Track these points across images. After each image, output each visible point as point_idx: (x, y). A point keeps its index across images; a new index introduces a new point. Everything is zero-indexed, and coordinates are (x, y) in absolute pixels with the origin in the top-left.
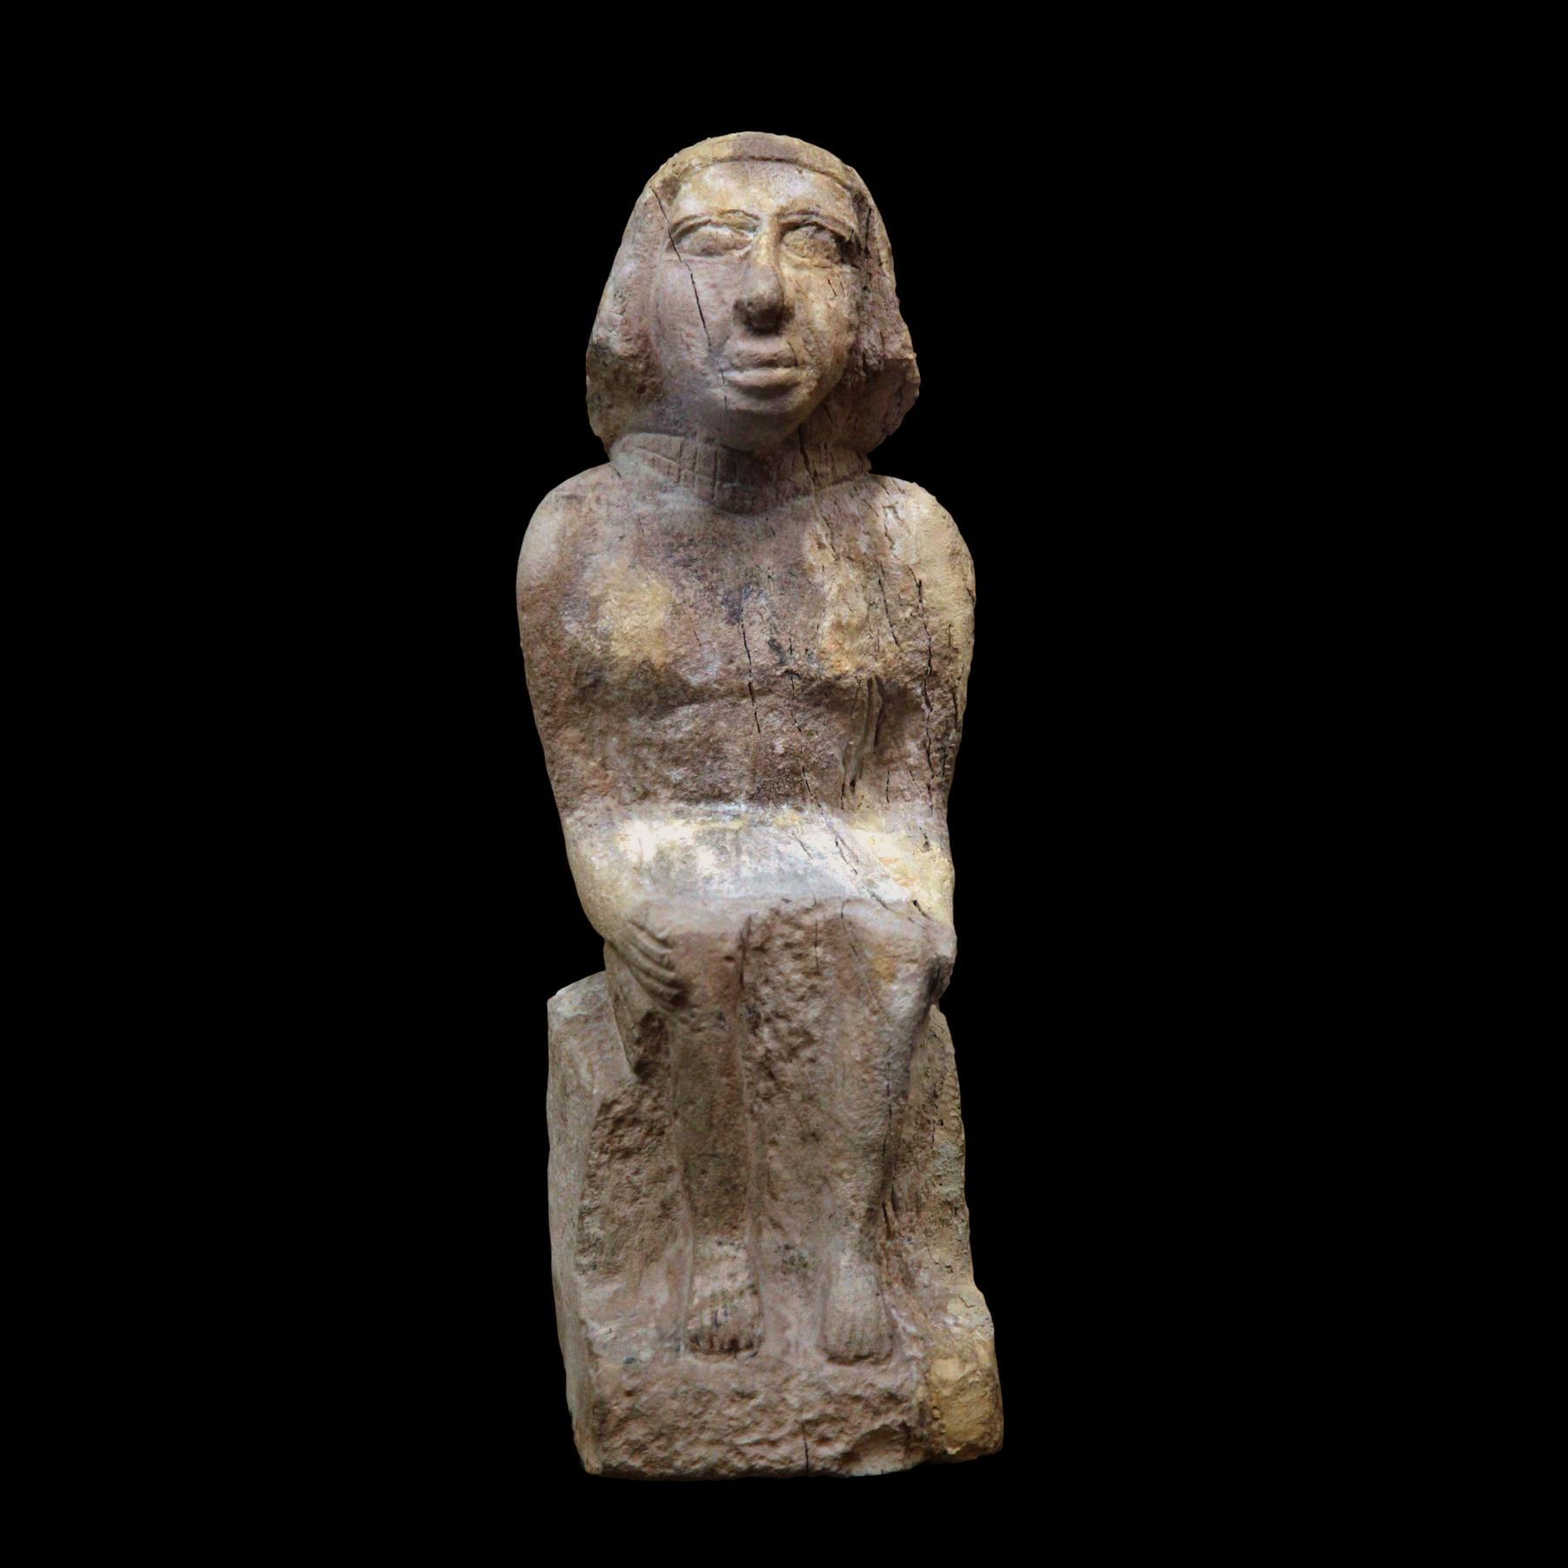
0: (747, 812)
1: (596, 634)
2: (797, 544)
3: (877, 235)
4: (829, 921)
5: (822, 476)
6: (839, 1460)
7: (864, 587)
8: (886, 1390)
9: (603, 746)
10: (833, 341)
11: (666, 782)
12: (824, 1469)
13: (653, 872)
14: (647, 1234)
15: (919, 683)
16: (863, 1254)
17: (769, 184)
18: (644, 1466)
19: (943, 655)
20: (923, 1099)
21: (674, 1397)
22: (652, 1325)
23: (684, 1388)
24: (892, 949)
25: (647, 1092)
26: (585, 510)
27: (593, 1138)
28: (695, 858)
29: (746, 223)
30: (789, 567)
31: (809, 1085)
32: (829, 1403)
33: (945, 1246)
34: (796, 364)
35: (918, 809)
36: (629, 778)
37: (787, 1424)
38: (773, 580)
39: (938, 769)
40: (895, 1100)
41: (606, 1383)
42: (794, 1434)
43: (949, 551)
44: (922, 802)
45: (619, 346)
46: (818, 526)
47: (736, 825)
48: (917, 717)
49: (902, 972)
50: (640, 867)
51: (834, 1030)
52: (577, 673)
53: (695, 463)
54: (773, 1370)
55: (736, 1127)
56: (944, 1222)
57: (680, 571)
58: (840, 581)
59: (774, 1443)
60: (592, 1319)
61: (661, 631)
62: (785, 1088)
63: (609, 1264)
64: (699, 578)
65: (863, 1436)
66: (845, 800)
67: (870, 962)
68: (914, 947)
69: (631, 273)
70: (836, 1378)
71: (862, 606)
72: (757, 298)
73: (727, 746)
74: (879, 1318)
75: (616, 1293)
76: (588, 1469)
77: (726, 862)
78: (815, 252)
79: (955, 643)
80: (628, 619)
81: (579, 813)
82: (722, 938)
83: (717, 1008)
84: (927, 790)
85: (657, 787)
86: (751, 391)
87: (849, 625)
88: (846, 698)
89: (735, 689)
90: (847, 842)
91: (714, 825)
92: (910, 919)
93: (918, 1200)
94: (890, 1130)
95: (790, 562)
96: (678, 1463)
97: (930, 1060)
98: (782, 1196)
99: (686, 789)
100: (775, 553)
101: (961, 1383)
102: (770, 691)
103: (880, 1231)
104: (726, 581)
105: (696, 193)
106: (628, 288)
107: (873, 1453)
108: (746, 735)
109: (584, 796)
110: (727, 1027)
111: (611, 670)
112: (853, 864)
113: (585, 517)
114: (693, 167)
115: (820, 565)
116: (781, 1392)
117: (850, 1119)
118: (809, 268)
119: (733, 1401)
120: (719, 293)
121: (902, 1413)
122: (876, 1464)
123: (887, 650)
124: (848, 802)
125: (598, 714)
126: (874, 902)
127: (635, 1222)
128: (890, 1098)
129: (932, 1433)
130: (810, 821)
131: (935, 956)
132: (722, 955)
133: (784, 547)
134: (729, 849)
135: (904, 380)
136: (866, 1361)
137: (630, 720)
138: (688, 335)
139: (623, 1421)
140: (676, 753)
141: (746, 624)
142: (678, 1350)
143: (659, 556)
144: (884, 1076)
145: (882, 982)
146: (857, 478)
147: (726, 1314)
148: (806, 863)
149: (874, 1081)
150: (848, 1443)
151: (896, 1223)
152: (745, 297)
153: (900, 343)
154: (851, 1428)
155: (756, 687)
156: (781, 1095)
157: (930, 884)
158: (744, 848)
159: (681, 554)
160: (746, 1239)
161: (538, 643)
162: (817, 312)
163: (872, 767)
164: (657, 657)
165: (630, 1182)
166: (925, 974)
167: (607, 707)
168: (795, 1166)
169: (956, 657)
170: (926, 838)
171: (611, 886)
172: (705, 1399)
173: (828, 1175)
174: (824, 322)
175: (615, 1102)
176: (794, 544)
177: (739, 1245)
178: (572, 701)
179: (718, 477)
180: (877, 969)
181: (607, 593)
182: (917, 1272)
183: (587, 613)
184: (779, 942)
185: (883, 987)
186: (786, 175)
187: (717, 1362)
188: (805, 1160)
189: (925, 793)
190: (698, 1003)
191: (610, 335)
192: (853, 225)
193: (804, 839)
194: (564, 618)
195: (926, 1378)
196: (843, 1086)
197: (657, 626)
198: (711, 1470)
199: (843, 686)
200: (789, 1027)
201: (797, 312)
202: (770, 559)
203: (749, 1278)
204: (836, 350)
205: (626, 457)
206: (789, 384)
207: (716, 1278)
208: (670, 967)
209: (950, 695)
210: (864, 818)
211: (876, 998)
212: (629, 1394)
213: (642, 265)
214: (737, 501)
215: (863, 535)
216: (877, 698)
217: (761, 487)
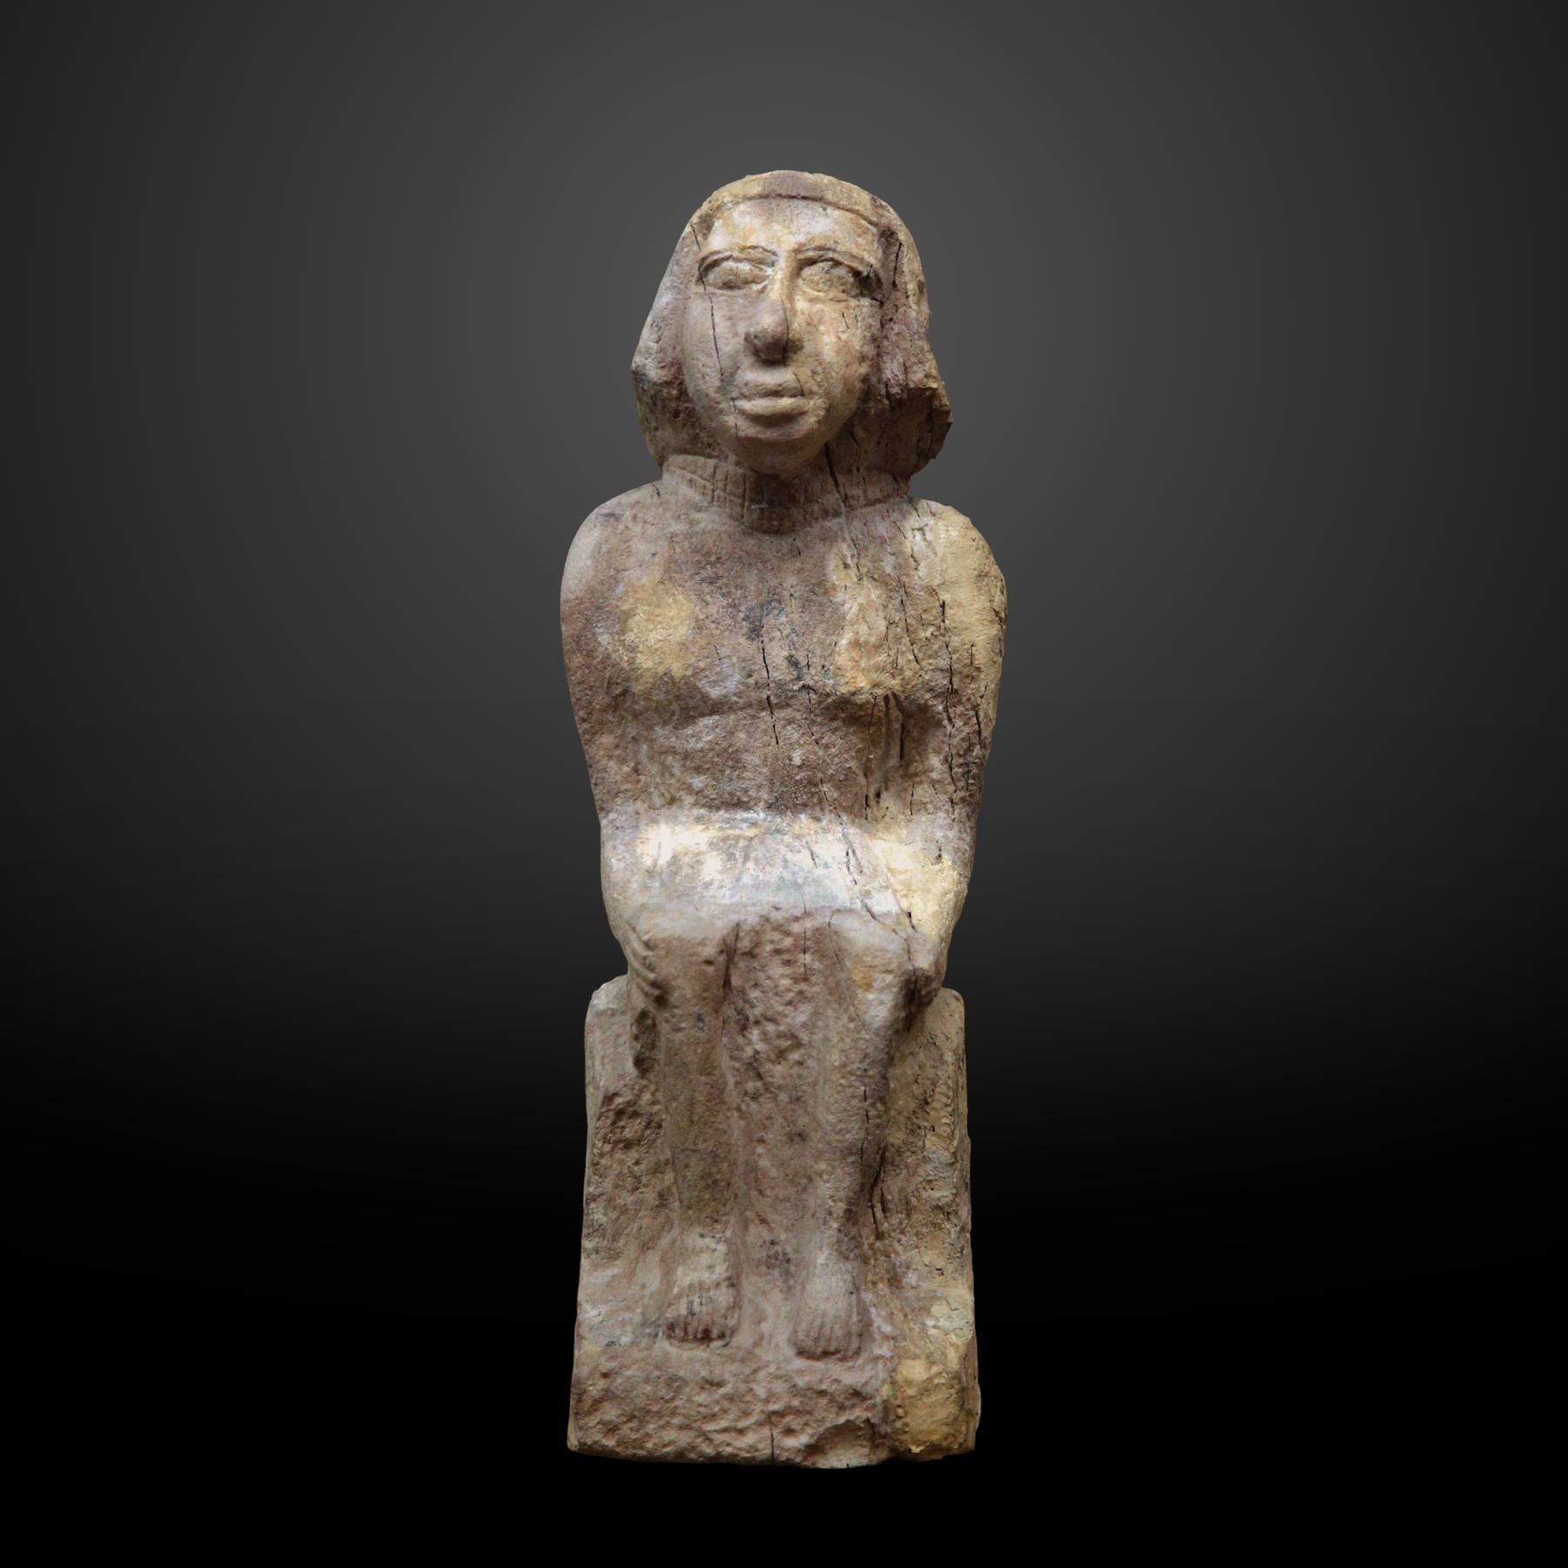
0: (765, 820)
2: (821, 564)
3: (906, 269)
4: (817, 930)
5: (853, 498)
6: (803, 1451)
7: (885, 607)
8: (851, 1386)
9: (636, 753)
10: (842, 372)
11: (689, 789)
12: (788, 1459)
13: (663, 875)
14: (645, 1222)
15: (940, 700)
16: (841, 1253)
17: (792, 221)
18: (618, 1445)
19: (964, 674)
20: (912, 1105)
21: (647, 1381)
22: (639, 1310)
23: (657, 1373)
24: (868, 959)
25: (646, 1086)
26: (621, 527)
27: (597, 1128)
29: (763, 259)
30: (811, 586)
31: (796, 1087)
32: (796, 1396)
33: (937, 1248)
34: (803, 394)
35: (940, 822)
36: (658, 784)
37: (754, 1414)
38: (795, 598)
39: (961, 784)
40: (873, 1105)
41: (584, 1364)
42: (761, 1424)
43: (976, 573)
44: (944, 815)
45: (654, 373)
46: (845, 546)
47: (751, 833)
48: (940, 733)
49: (878, 981)
50: (653, 871)
51: (820, 1035)
52: (609, 683)
53: (726, 485)
54: (743, 1360)
56: (936, 1226)
57: (706, 588)
58: (861, 600)
59: (741, 1432)
60: (587, 1302)
61: (683, 645)
62: (772, 1089)
63: (610, 1249)
64: (723, 595)
65: (827, 1430)
66: (869, 811)
67: (849, 970)
68: (890, 958)
69: (667, 304)
70: (803, 1372)
71: (882, 625)
72: (762, 332)
73: (746, 757)
74: (850, 1316)
75: (613, 1277)
76: (569, 1445)
77: (730, 869)
78: (831, 286)
79: (977, 662)
80: (654, 632)
81: (612, 816)
82: (703, 943)
83: (696, 1009)
84: (950, 803)
85: (681, 793)
86: (757, 419)
87: (867, 643)
88: (862, 713)
89: (754, 702)
90: (858, 853)
91: (730, 832)
92: (894, 931)
93: (908, 1203)
94: (868, 1134)
95: (813, 581)
96: (649, 1445)
97: (920, 1067)
98: (768, 1192)
100: (799, 572)
101: (926, 1384)
102: (788, 705)
103: (866, 1231)
104: (749, 598)
105: (724, 229)
106: (664, 318)
107: (839, 1446)
108: (764, 746)
109: (617, 799)
110: (705, 1028)
111: (637, 680)
112: (855, 875)
113: (621, 534)
114: (725, 204)
115: (843, 584)
116: (748, 1382)
117: (828, 1122)
118: (824, 302)
119: (703, 1388)
120: (734, 325)
121: (867, 1409)
122: (842, 1458)
123: (905, 667)
124: (872, 813)
125: (629, 722)
126: (864, 912)
127: (635, 1210)
128: (867, 1103)
129: (896, 1431)
130: (826, 831)
131: (911, 968)
132: (700, 959)
133: (808, 567)
134: (737, 856)
135: (931, 408)
136: (833, 1357)
137: (656, 728)
139: (597, 1403)
140: (697, 762)
141: (766, 639)
142: (656, 1335)
143: (687, 573)
144: (861, 1081)
145: (859, 992)
146: (892, 500)
148: (809, 872)
149: (851, 1086)
150: (812, 1436)
151: (886, 1225)
152: (752, 330)
154: (817, 1421)
155: (774, 700)
156: (769, 1095)
157: (931, 896)
158: (753, 855)
159: (709, 571)
160: (728, 1233)
161: (574, 653)
162: (827, 344)
163: (899, 780)
164: (677, 669)
165: (631, 1172)
166: (900, 985)
167: (636, 715)
168: (782, 1164)
169: (978, 676)
170: (940, 850)
171: (622, 888)
172: (676, 1384)
175: (616, 1094)
176: (819, 564)
177: (720, 1238)
178: (603, 710)
179: (747, 498)
180: (855, 978)
181: (636, 608)
182: (905, 1273)
183: (618, 626)
184: (769, 948)
185: (859, 996)
186: (810, 212)
187: (691, 1349)
188: (791, 1159)
189: (948, 806)
190: (677, 1004)
191: (647, 362)
192: (872, 260)
193: (816, 848)
195: (891, 1377)
197: (679, 640)
198: (681, 1454)
199: (859, 702)
200: (777, 1030)
201: (806, 344)
202: (794, 578)
203: (727, 1269)
204: (845, 380)
205: (669, 477)
206: (795, 412)
207: (695, 1270)
208: (651, 968)
209: (972, 713)
210: (887, 829)
211: (854, 1005)
212: (605, 1376)
213: (679, 296)
214: (765, 522)
215: (889, 556)
216: (895, 713)
217: (788, 509)
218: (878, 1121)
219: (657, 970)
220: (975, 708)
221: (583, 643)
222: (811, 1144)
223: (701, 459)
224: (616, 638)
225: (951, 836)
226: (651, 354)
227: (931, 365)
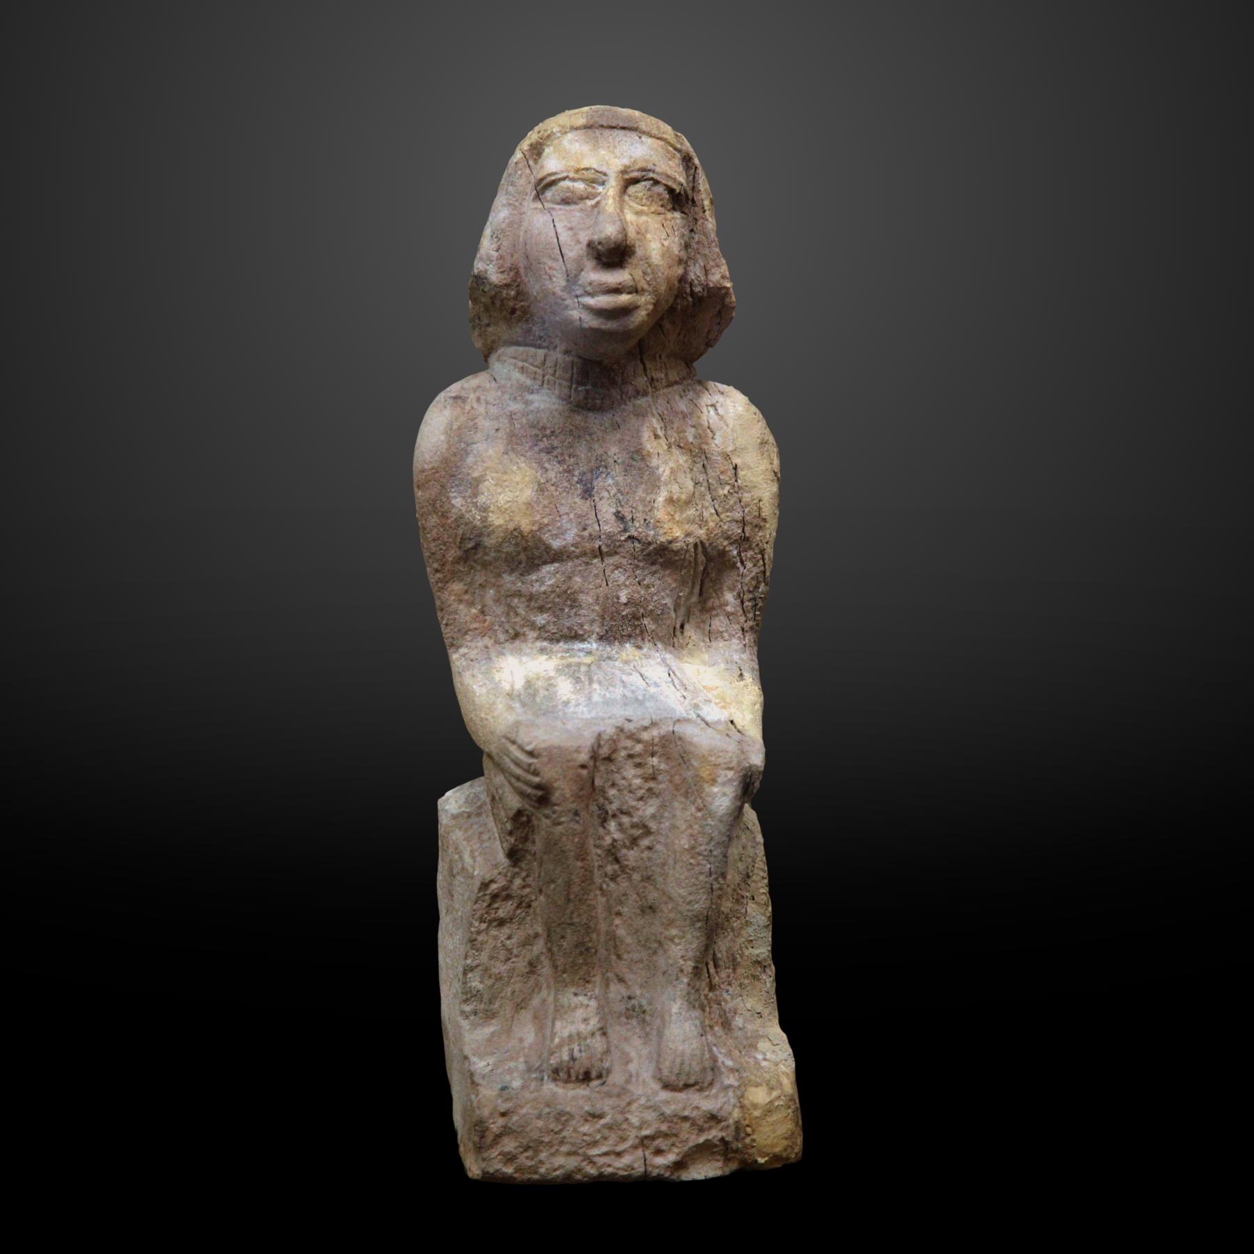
0: (597, 649)
1: (476, 507)
2: (637, 435)
3: (701, 188)
4: (663, 737)
5: (657, 381)
6: (671, 1168)
7: (691, 470)
8: (709, 1112)
9: (482, 597)
10: (666, 273)
11: (533, 626)
12: (659, 1175)
13: (522, 697)
14: (517, 987)
15: (735, 546)
16: (690, 1003)
17: (615, 147)
18: (515, 1172)
19: (754, 524)
20: (738, 879)
21: (539, 1117)
22: (522, 1060)
23: (547, 1110)
24: (713, 759)
25: (517, 873)
26: (468, 408)
27: (474, 910)
29: (597, 178)
30: (631, 454)
31: (647, 868)
32: (663, 1122)
33: (755, 996)
34: (636, 291)
35: (734, 647)
36: (503, 622)
37: (629, 1139)
38: (618, 464)
39: (751, 615)
40: (716, 879)
41: (485, 1106)
42: (635, 1147)
43: (759, 441)
44: (738, 642)
45: (495, 277)
46: (654, 421)
47: (588, 660)
48: (734, 574)
49: (722, 777)
50: (512, 694)
51: (667, 824)
52: (461, 539)
53: (555, 371)
54: (619, 1096)
56: (755, 977)
57: (544, 456)
58: (672, 464)
59: (619, 1154)
60: (474, 1055)
61: (529, 505)
62: (628, 870)
63: (487, 1011)
64: (559, 462)
65: (690, 1148)
66: (675, 640)
67: (696, 769)
68: (731, 758)
69: (504, 219)
70: (669, 1102)
71: (690, 485)
72: (606, 239)
73: (582, 597)
74: (703, 1054)
75: (493, 1034)
76: (470, 1175)
77: (580, 689)
78: (652, 201)
79: (764, 514)
80: (502, 495)
81: (463, 650)
82: (578, 750)
83: (573, 806)
84: (741, 632)
85: (525, 629)
86: (600, 313)
87: (679, 500)
88: (677, 558)
89: (588, 551)
90: (677, 674)
91: (571, 660)
92: (728, 735)
93: (734, 959)
94: (712, 903)
95: (632, 449)
96: (542, 1170)
97: (744, 848)
98: (625, 956)
100: (620, 442)
101: (768, 1106)
102: (616, 553)
103: (704, 984)
104: (581, 465)
105: (557, 154)
106: (502, 230)
107: (698, 1162)
108: (596, 588)
109: (467, 636)
110: (581, 821)
111: (489, 536)
112: (682, 691)
113: (468, 413)
114: (554, 134)
115: (656, 452)
116: (624, 1113)
117: (680, 895)
118: (647, 215)
119: (586, 1120)
120: (575, 234)
121: (721, 1130)
122: (701, 1171)
123: (709, 520)
124: (678, 641)
125: (478, 571)
126: (699, 721)
127: (508, 977)
128: (712, 878)
129: (745, 1146)
130: (647, 657)
131: (747, 765)
132: (578, 764)
133: (627, 438)
134: (583, 679)
135: (723, 304)
136: (693, 1088)
137: (504, 576)
138: (550, 268)
139: (498, 1137)
140: (540, 602)
141: (597, 499)
142: (542, 1079)
143: (527, 445)
144: (707, 860)
145: (706, 786)
146: (685, 382)
147: (580, 1051)
148: (645, 690)
149: (699, 864)
150: (678, 1154)
151: (717, 978)
152: (596, 237)
154: (681, 1142)
155: (604, 549)
156: (625, 876)
157: (744, 707)
158: (595, 678)
159: (545, 443)
160: (597, 991)
161: (430, 514)
162: (654, 250)
163: (697, 613)
164: (526, 525)
165: (504, 945)
166: (739, 779)
167: (485, 565)
168: (636, 932)
169: (765, 526)
170: (741, 670)
171: (488, 709)
172: (564, 1119)
174: (659, 257)
175: (492, 881)
176: (635, 435)
177: (591, 995)
178: (457, 561)
179: (574, 381)
180: (702, 775)
181: (485, 474)
182: (733, 1017)
183: (470, 490)
184: (623, 753)
185: (706, 789)
186: (629, 140)
187: (573, 1089)
188: (643, 928)
189: (740, 634)
190: (558, 802)
191: (488, 268)
193: (643, 671)
194: (451, 494)
195: (740, 1102)
196: (674, 868)
197: (525, 501)
198: (568, 1176)
199: (674, 549)
200: (631, 822)
201: (637, 249)
202: (616, 447)
203: (599, 1022)
204: (668, 280)
205: (501, 366)
206: (631, 307)
207: (573, 1022)
208: (536, 773)
209: (759, 556)
210: (691, 654)
211: (701, 798)
212: (503, 1115)
213: (514, 212)
214: (590, 401)
215: (690, 428)
216: (701, 558)
217: (608, 390)
218: (720, 892)
219: (541, 774)
220: (762, 552)
221: (438, 505)
222: (660, 914)
225: (745, 658)
226: (491, 261)
227: (724, 269)
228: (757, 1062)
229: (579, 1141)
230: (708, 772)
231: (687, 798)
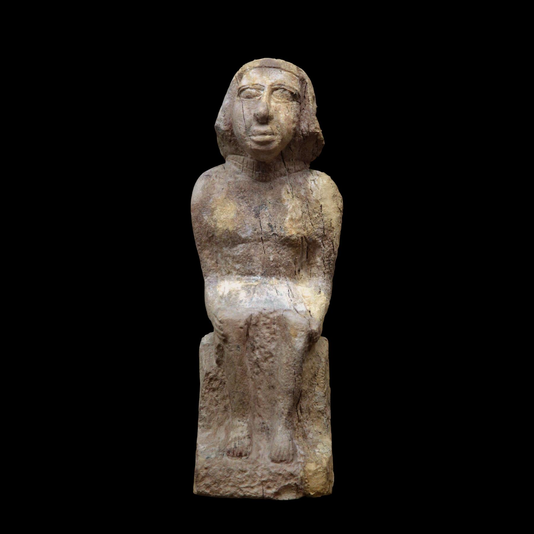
0: (260, 279)
2: (280, 192)
3: (308, 91)
4: (278, 317)
5: (290, 169)
6: (274, 494)
7: (302, 207)
8: (290, 472)
9: (217, 256)
10: (287, 127)
11: (235, 269)
12: (268, 497)
13: (226, 298)
14: (220, 416)
15: (320, 238)
16: (286, 427)
17: (270, 75)
18: (210, 492)
19: (328, 229)
20: (311, 376)
21: (220, 470)
22: (218, 446)
23: (224, 468)
24: (296, 327)
25: (220, 370)
26: (212, 179)
27: (203, 384)
28: (239, 294)
29: (260, 88)
30: (276, 200)
31: (271, 370)
32: (271, 475)
33: (319, 425)
34: (273, 134)
35: (320, 280)
36: (224, 267)
37: (257, 481)
38: (271, 204)
39: (327, 267)
40: (297, 376)
41: (199, 465)
42: (259, 485)
43: (332, 195)
44: (322, 278)
46: (288, 186)
47: (256, 284)
48: (320, 250)
49: (299, 334)
50: (223, 297)
51: (279, 353)
52: (207, 232)
53: (247, 165)
54: (253, 463)
55: (244, 383)
56: (319, 417)
57: (240, 200)
58: (293, 204)
59: (252, 488)
60: (200, 443)
61: (233, 220)
62: (263, 371)
63: (208, 425)
64: (246, 203)
65: (282, 487)
66: (296, 276)
67: (289, 330)
68: (303, 326)
69: (227, 104)
70: (273, 467)
71: (300, 213)
72: (259, 113)
73: (254, 258)
74: (289, 448)
75: (209, 435)
76: (194, 492)
77: (249, 296)
78: (283, 97)
79: (333, 226)
80: (223, 215)
81: (208, 278)
82: (239, 321)
83: (237, 344)
84: (323, 274)
85: (232, 270)
86: (258, 143)
87: (295, 219)
88: (294, 243)
89: (257, 239)
90: (292, 290)
91: (249, 283)
92: (304, 317)
93: (309, 410)
94: (296, 386)
95: (277, 198)
96: (221, 492)
97: (313, 363)
98: (262, 406)
99: (241, 271)
100: (272, 195)
101: (315, 471)
102: (268, 240)
103: (295, 419)
104: (255, 204)
105: (246, 78)
106: (226, 108)
107: (286, 492)
108: (260, 254)
109: (210, 272)
110: (240, 350)
111: (217, 232)
112: (291, 298)
113: (212, 182)
114: (247, 70)
115: (287, 199)
116: (255, 471)
117: (282, 382)
118: (280, 103)
119: (240, 473)
120: (250, 111)
121: (295, 480)
122: (287, 496)
123: (308, 227)
124: (297, 277)
125: (214, 246)
126: (294, 311)
127: (216, 412)
128: (295, 376)
129: (305, 488)
130: (281, 283)
131: (310, 330)
132: (238, 327)
133: (275, 193)
134: (251, 292)
135: (317, 139)
136: (284, 462)
137: (224, 248)
139: (203, 478)
140: (237, 260)
141: (261, 218)
142: (223, 455)
143: (234, 195)
144: (293, 368)
145: (293, 338)
146: (304, 170)
147: (239, 444)
148: (275, 297)
149: (290, 370)
150: (276, 489)
151: (302, 417)
152: (256, 112)
153: (315, 126)
154: (278, 484)
155: (264, 238)
156: (262, 373)
157: (317, 305)
158: (256, 291)
159: (242, 194)
160: (248, 420)
161: (196, 222)
162: (281, 117)
163: (306, 266)
164: (231, 228)
165: (215, 399)
166: (306, 335)
167: (217, 244)
168: (266, 397)
169: (333, 230)
170: (320, 290)
171: (212, 302)
172: (230, 471)
173: (277, 400)
175: (210, 373)
176: (279, 192)
177: (245, 422)
178: (205, 242)
179: (254, 170)
180: (291, 333)
181: (217, 207)
182: (308, 434)
183: (210, 213)
184: (262, 323)
185: (293, 339)
186: (276, 72)
187: (235, 460)
188: (269, 395)
189: (323, 275)
190: (231, 342)
191: (220, 123)
193: (278, 289)
195: (303, 469)
196: (280, 371)
197: (231, 218)
198: (232, 495)
199: (292, 239)
200: (265, 351)
201: (274, 117)
202: (270, 197)
203: (248, 432)
204: (288, 129)
206: (271, 140)
207: (237, 432)
208: (222, 330)
209: (331, 243)
210: (302, 282)
211: (291, 342)
212: (206, 468)
213: (231, 101)
214: (261, 178)
215: (303, 189)
216: (305, 243)
217: (268, 173)
219: (224, 330)
220: (332, 241)
222: (276, 389)
223: (239, 156)
224: (210, 217)
226: (222, 121)
228: (315, 452)
229: (236, 481)
230: (293, 332)
231: (286, 342)
